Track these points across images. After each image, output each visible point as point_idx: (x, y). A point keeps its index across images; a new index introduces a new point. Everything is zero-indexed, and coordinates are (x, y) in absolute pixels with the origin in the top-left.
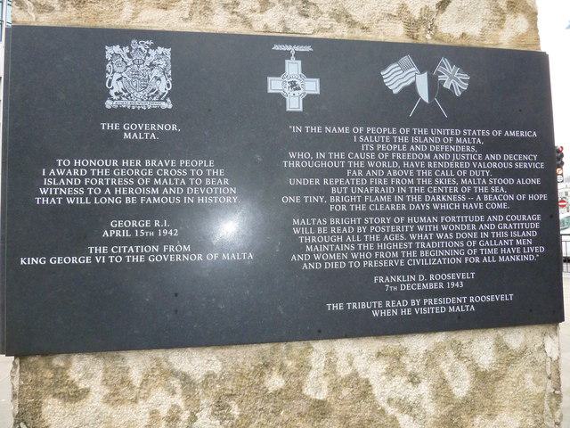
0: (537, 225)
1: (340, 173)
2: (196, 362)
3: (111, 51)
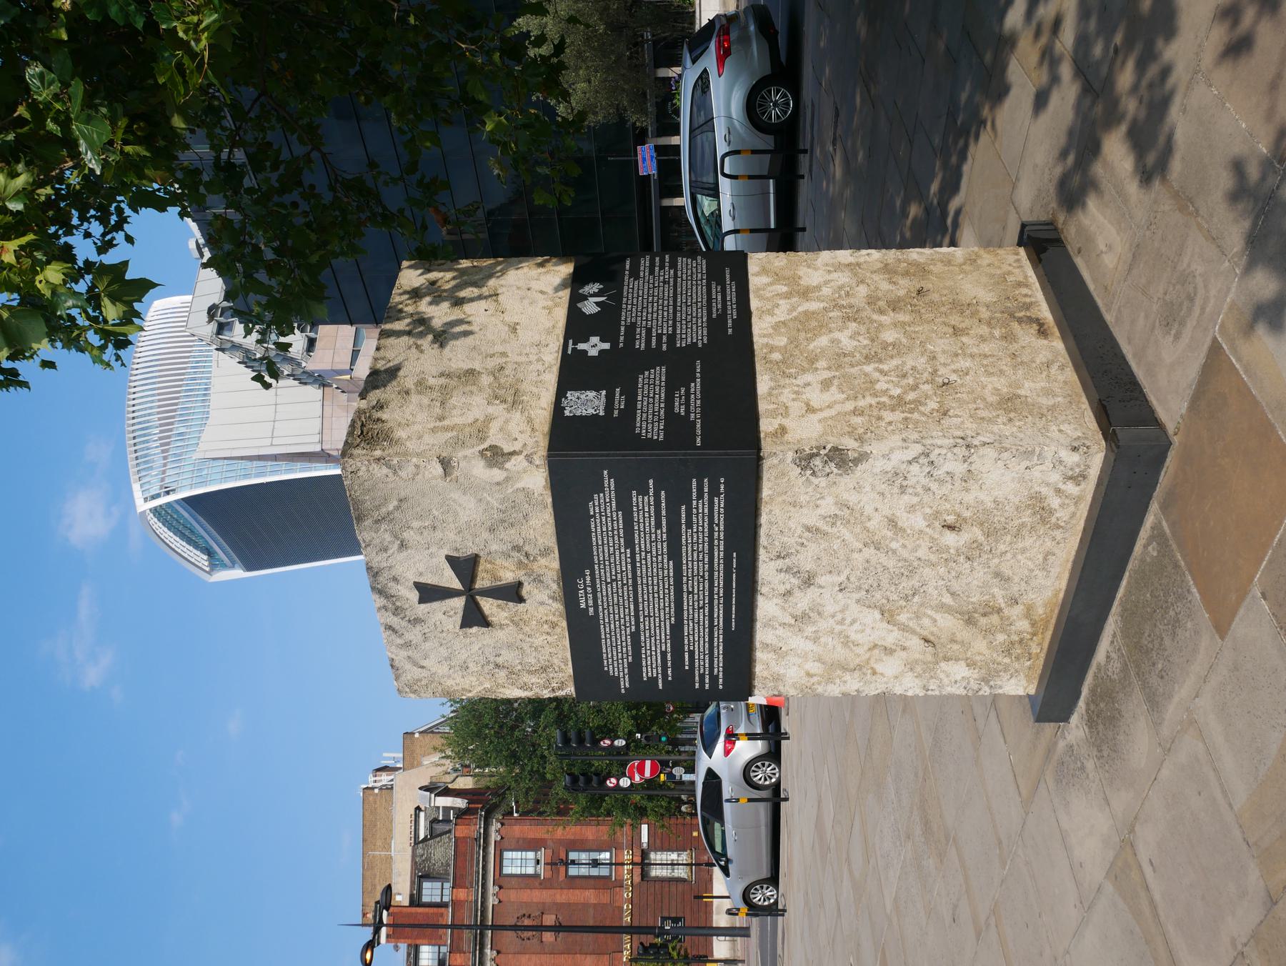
0: (685, 259)
1: (649, 331)
2: (1241, 611)
3: (567, 413)
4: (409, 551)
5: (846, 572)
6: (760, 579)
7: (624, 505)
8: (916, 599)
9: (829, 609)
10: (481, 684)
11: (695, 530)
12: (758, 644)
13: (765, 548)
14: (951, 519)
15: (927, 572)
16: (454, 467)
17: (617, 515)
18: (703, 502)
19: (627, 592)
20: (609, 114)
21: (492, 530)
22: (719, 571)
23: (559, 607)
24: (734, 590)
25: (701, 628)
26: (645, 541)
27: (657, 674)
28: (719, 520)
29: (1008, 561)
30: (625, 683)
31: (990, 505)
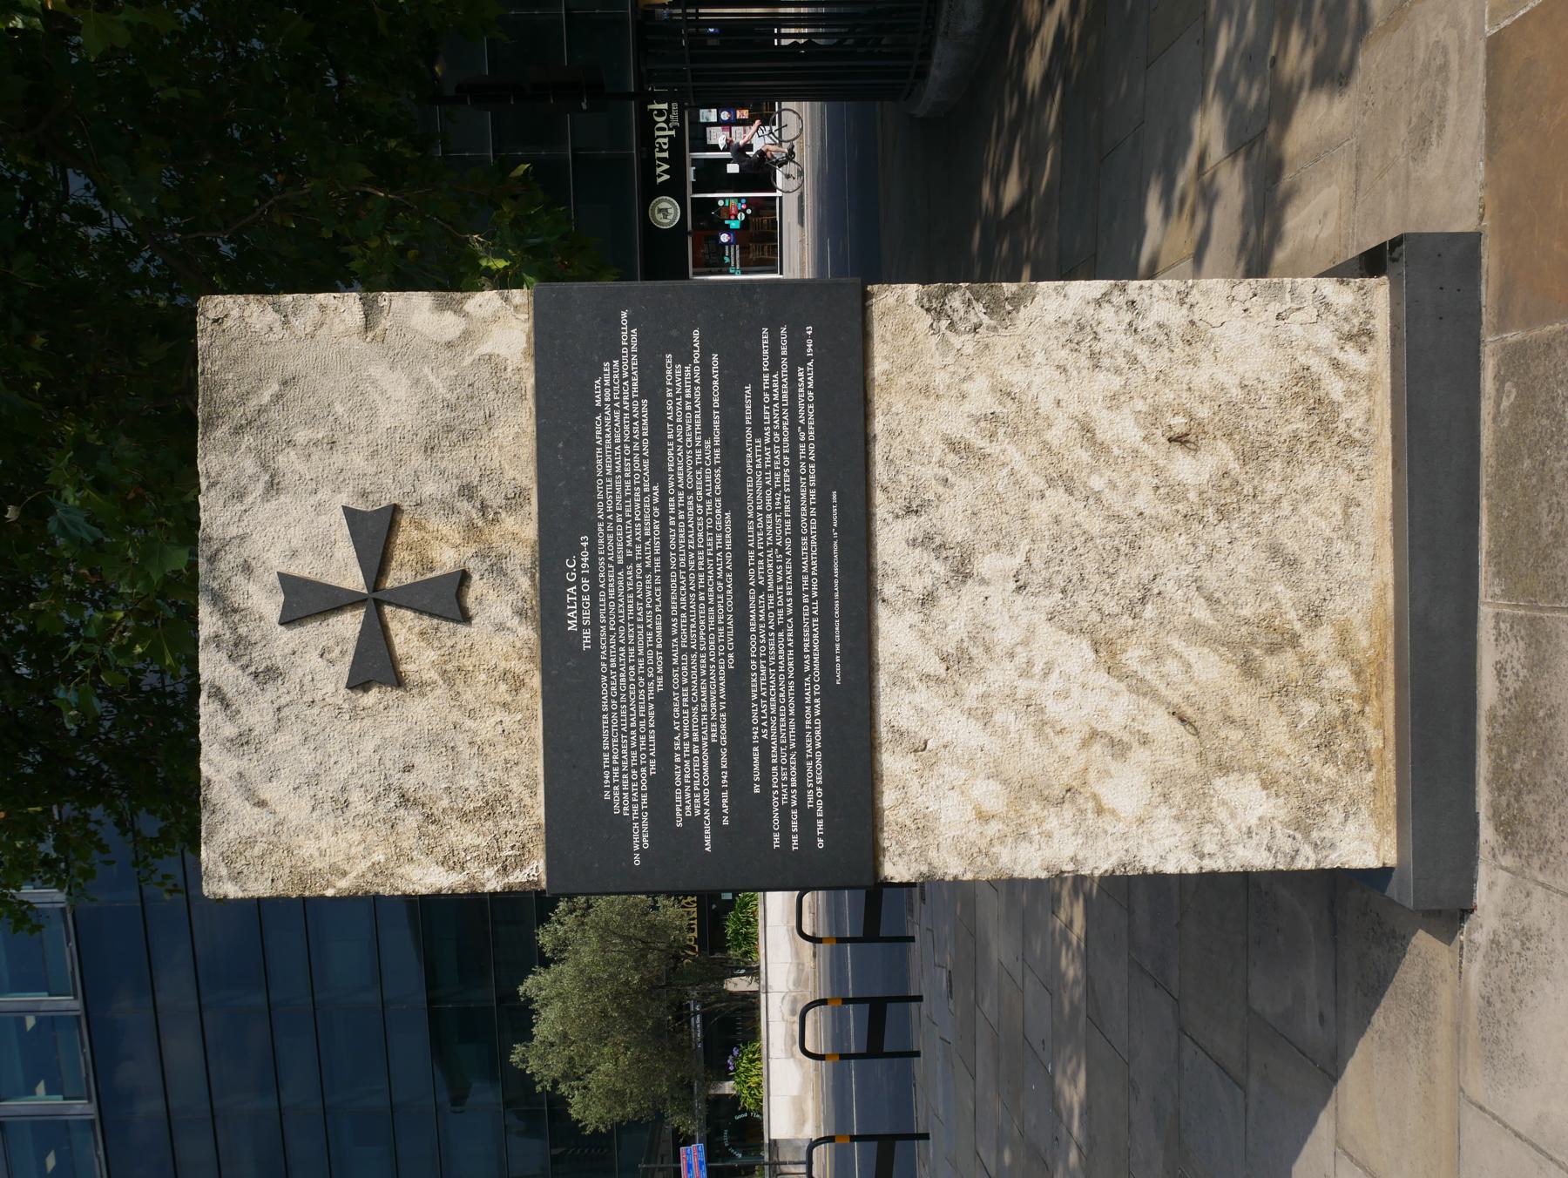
4: (282, 498)
5: (1024, 545)
6: (880, 563)
7: (652, 387)
8: (1149, 611)
9: (1005, 636)
10: (368, 852)
11: (768, 441)
12: (884, 733)
13: (885, 489)
14: (1179, 423)
15: (1157, 544)
16: (381, 311)
17: (640, 407)
18: (780, 378)
19: (650, 588)
20: (642, 1109)
21: (429, 449)
22: (809, 535)
23: (527, 633)
24: (836, 582)
25: (782, 678)
26: (685, 467)
27: (703, 807)
28: (806, 416)
29: (1287, 518)
30: (641, 838)
31: (1236, 393)
